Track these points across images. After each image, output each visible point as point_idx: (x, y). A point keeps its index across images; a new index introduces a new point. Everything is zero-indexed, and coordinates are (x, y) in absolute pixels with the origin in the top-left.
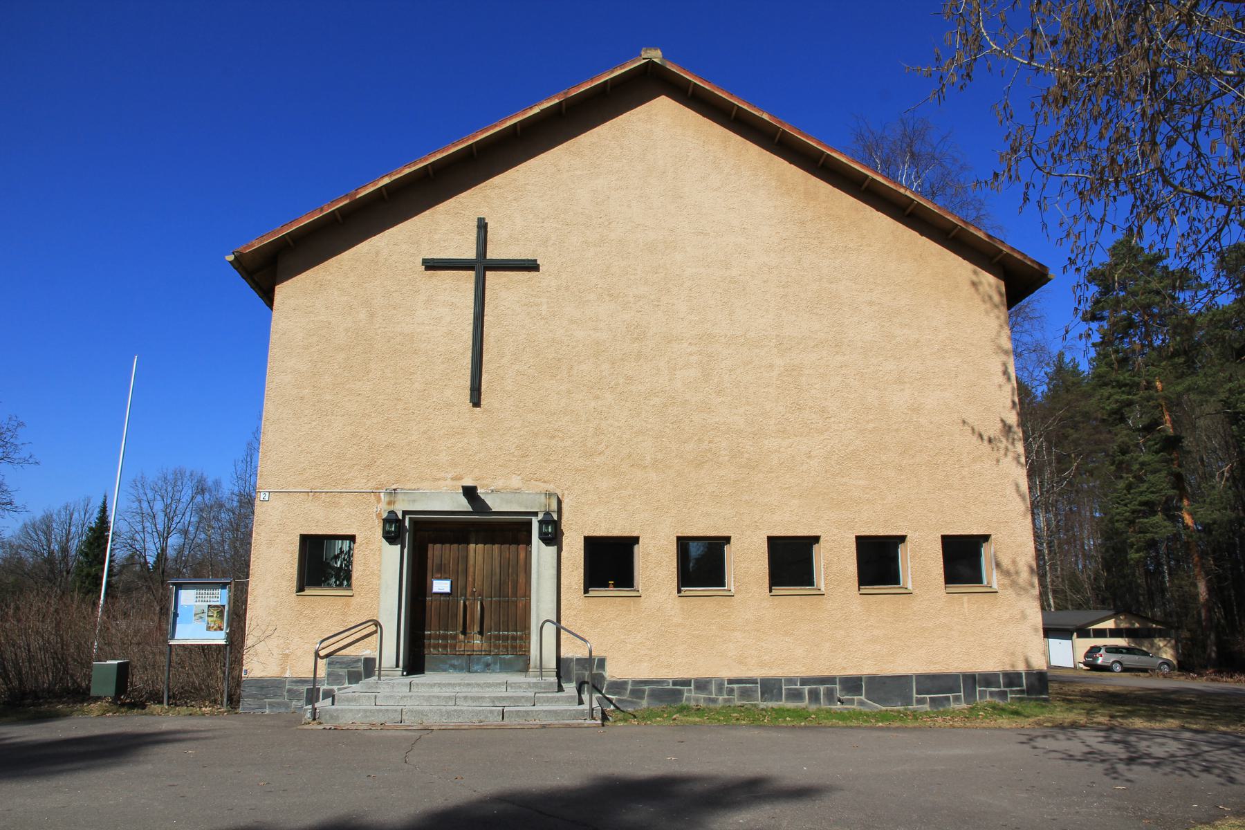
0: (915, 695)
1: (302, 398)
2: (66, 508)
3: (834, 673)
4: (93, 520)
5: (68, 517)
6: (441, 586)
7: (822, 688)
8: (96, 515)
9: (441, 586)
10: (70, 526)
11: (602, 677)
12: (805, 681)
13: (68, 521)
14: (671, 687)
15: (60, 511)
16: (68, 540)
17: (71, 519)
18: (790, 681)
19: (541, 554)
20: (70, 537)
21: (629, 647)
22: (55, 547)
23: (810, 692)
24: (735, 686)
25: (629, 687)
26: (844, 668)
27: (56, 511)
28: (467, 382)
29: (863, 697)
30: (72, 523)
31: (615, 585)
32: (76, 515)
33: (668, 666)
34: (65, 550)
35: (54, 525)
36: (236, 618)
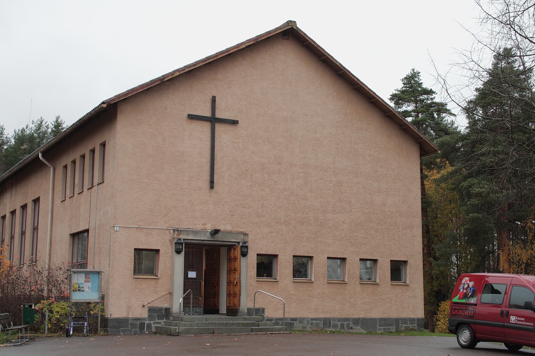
0: (378, 327)
3: (350, 317)
12: (339, 320)
18: (334, 319)
24: (313, 321)
28: (207, 178)
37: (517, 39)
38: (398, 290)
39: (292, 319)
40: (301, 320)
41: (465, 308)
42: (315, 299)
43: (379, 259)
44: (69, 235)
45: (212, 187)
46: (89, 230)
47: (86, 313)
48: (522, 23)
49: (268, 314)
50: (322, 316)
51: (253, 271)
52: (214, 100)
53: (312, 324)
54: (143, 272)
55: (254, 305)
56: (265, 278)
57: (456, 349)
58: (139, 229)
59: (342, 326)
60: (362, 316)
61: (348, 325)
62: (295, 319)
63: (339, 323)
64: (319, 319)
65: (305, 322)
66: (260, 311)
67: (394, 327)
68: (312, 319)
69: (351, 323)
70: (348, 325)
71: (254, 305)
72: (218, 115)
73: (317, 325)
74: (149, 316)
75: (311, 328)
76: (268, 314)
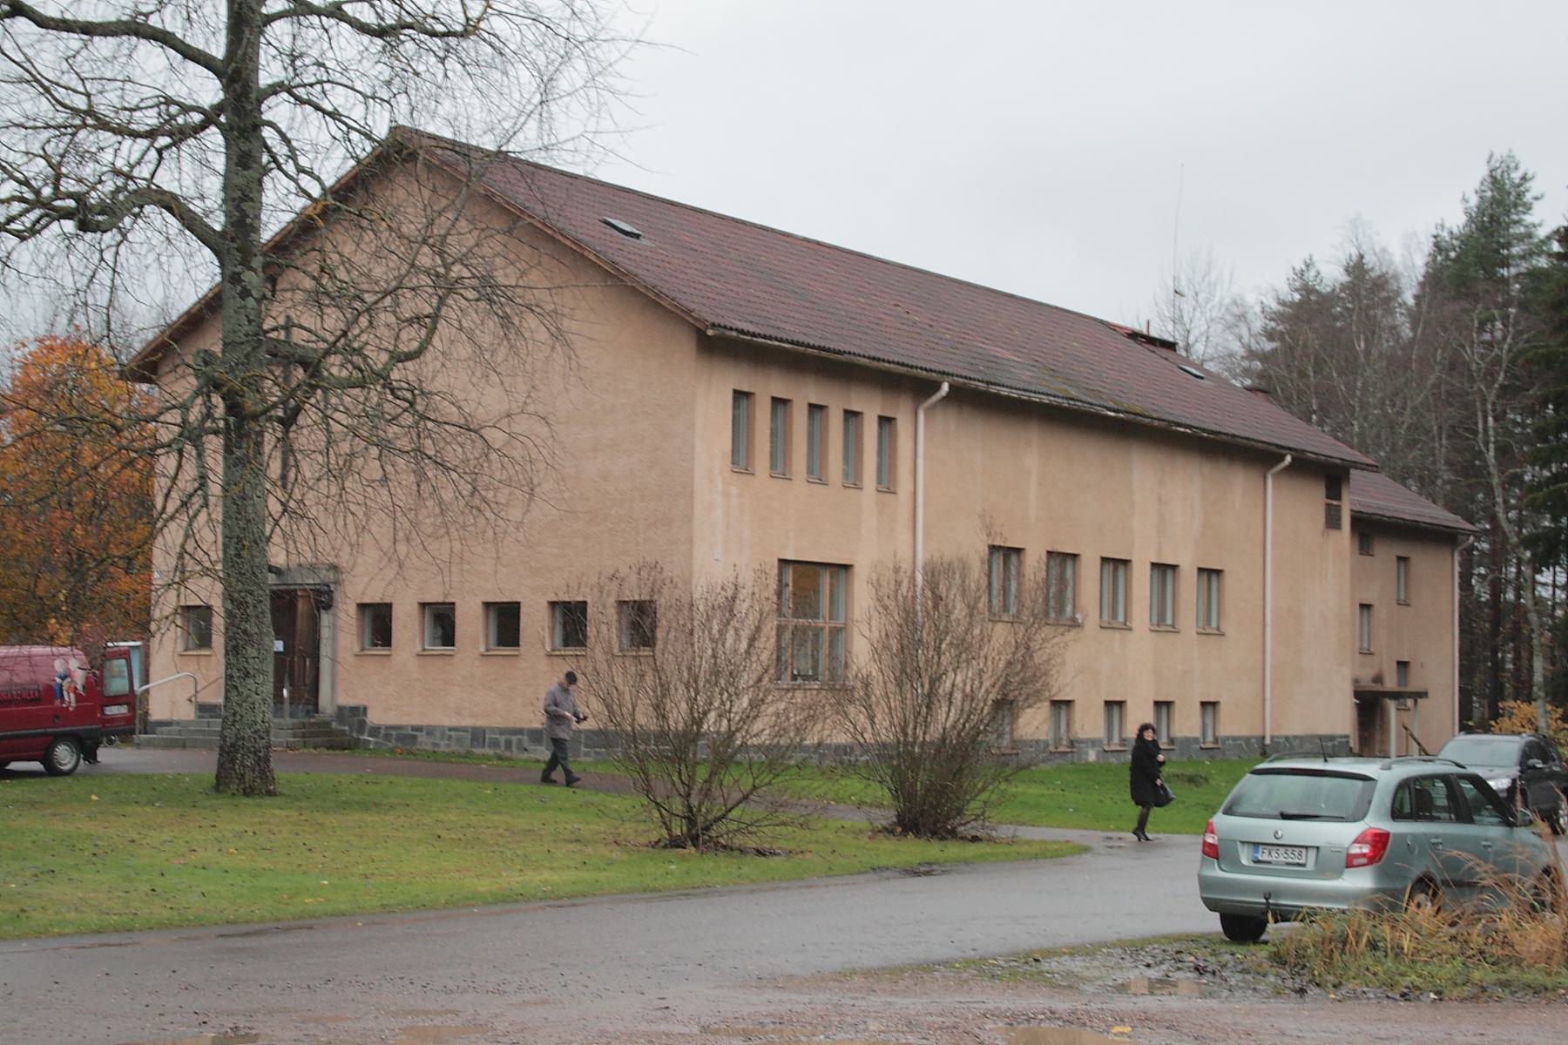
12: (502, 731)
18: (492, 730)
24: (453, 733)
37: (348, 272)
39: (415, 729)
40: (430, 731)
41: (619, 50)
43: (589, 601)
46: (566, 604)
47: (1382, 454)
48: (499, 360)
49: (373, 718)
50: (468, 722)
53: (450, 737)
54: (1330, 501)
57: (1178, 948)
59: (508, 744)
61: (520, 742)
62: (419, 729)
63: (502, 739)
64: (464, 729)
65: (438, 734)
66: (358, 712)
68: (451, 729)
69: (526, 738)
70: (520, 742)
73: (459, 740)
75: (448, 745)
76: (373, 718)
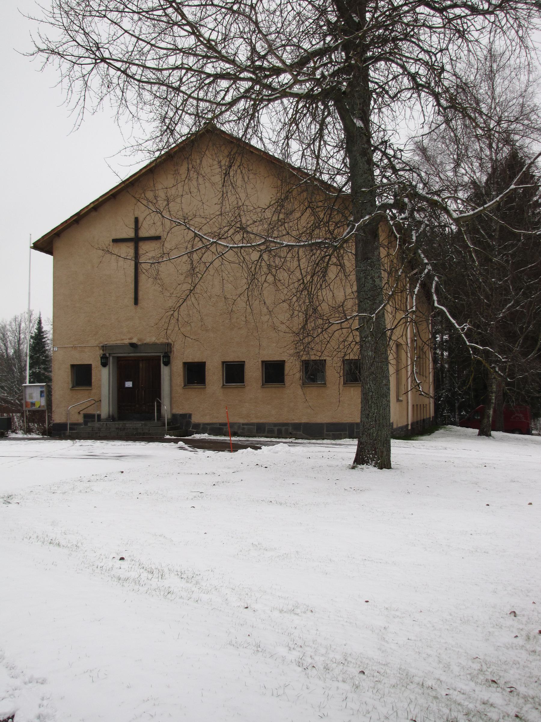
0: (325, 432)
1: (68, 306)
2: (15, 319)
3: (289, 422)
4: (34, 330)
5: (18, 327)
6: (129, 384)
7: (283, 429)
8: (36, 326)
9: (129, 384)
10: (20, 334)
11: (190, 422)
12: (275, 425)
13: (18, 330)
14: (218, 426)
15: (11, 323)
16: (19, 344)
17: (20, 327)
18: (269, 424)
19: (165, 371)
20: (21, 342)
21: (201, 409)
22: (11, 351)
23: (278, 430)
24: (245, 426)
25: (201, 426)
26: (293, 420)
27: (8, 323)
28: (132, 295)
29: (301, 433)
30: (21, 332)
31: (197, 383)
32: (23, 325)
33: (217, 418)
34: (18, 352)
35: (9, 334)
36: (48, 394)
38: (352, 392)
42: (246, 404)
44: (69, 367)
45: (136, 302)
50: (255, 421)
51: (179, 379)
52: (137, 220)
55: (137, 255)
56: (20, 436)
58: (74, 348)
60: (304, 420)
63: (276, 429)
67: (347, 432)
68: (243, 424)
69: (290, 428)
71: (137, 255)
72: (143, 233)
74: (84, 421)
